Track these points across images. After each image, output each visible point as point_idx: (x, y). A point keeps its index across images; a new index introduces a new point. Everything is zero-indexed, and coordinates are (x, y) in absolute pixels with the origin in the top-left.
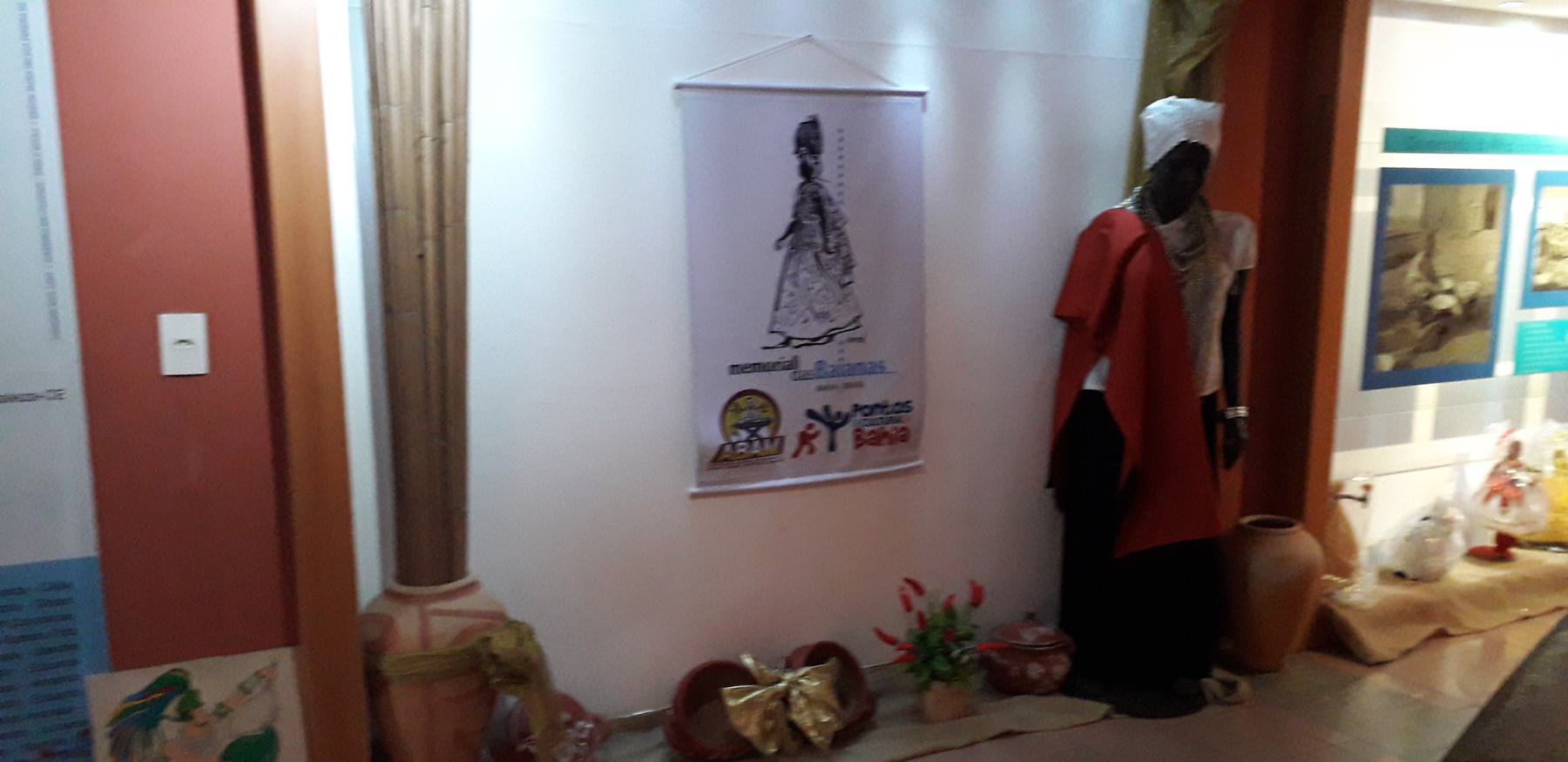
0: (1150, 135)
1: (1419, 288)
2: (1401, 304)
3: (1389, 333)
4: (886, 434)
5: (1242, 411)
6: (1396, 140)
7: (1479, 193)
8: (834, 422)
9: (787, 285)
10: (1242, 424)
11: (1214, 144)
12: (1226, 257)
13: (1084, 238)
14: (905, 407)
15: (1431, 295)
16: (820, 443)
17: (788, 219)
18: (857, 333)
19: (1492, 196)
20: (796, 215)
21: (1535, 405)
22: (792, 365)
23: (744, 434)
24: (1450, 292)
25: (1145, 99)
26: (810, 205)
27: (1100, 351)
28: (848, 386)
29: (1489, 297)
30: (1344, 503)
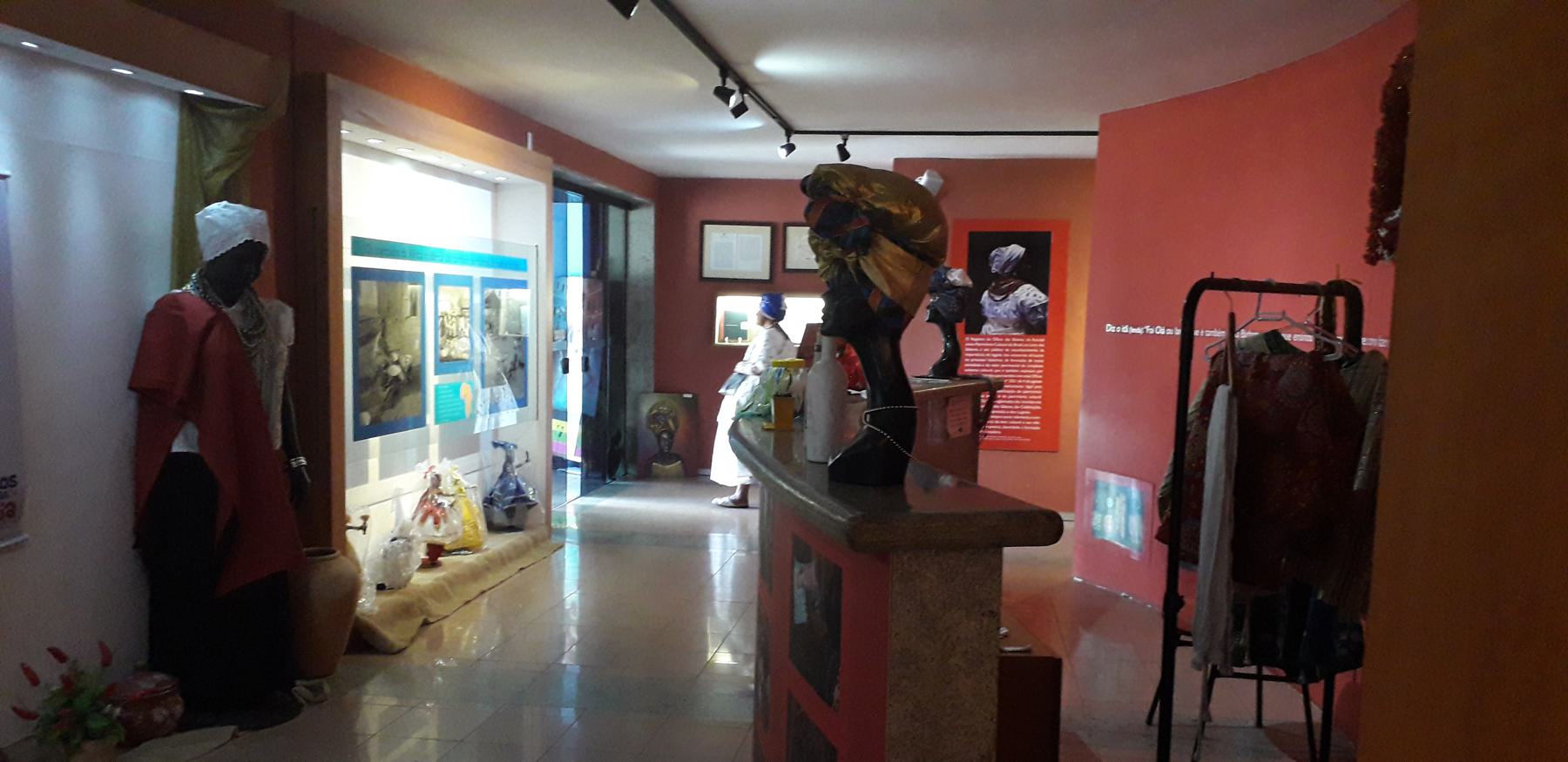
1: (380, 360)
2: (371, 372)
3: (366, 395)
5: (303, 461)
11: (267, 240)
15: (387, 366)
21: (434, 448)
24: (397, 363)
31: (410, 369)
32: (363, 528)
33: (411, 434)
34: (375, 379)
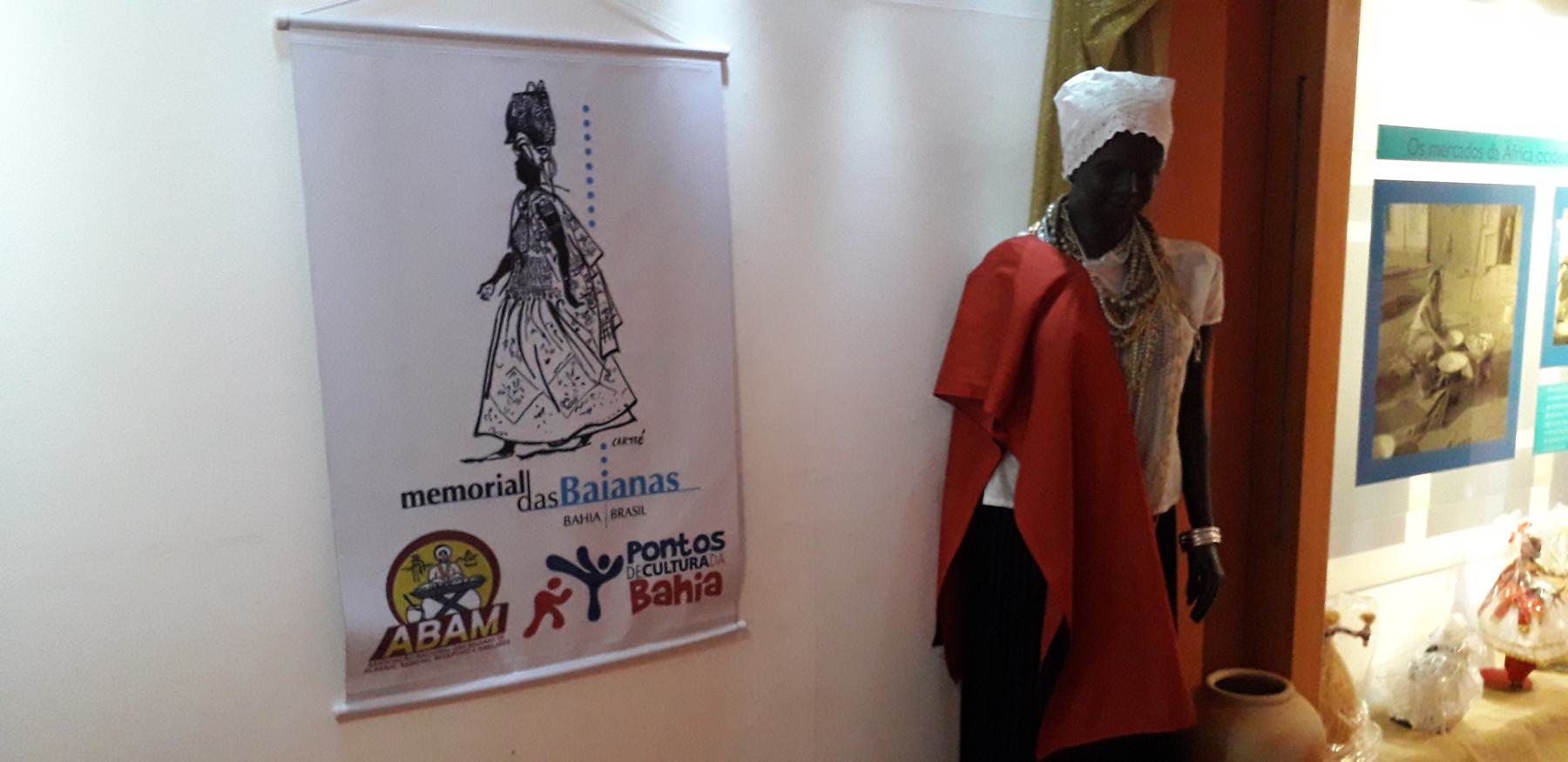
0: (1067, 124)
1: (1426, 343)
2: (1403, 366)
3: (1391, 405)
4: (687, 586)
5: (1215, 535)
6: (1393, 143)
7: (1492, 217)
8: (595, 573)
9: (503, 356)
10: (1214, 552)
12: (1184, 306)
13: (974, 279)
14: (716, 541)
15: (1438, 353)
16: (575, 609)
17: (503, 250)
18: (632, 431)
19: (1507, 221)
20: (512, 242)
21: (1540, 493)
22: (519, 486)
23: (432, 607)
24: (1462, 348)
25: (1056, 76)
26: (539, 226)
27: (1005, 450)
28: (617, 514)
29: (1508, 354)
30: (1339, 641)
31: (1488, 358)
32: (1365, 636)
33: (1493, 471)
34: (1412, 375)
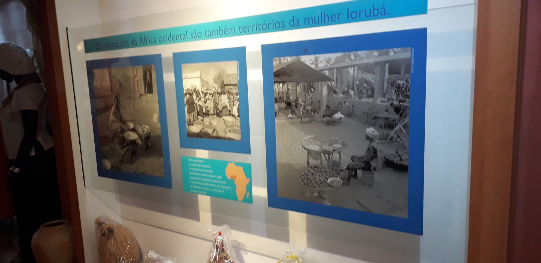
1: (117, 126)
6: (91, 45)
15: (123, 131)
19: (147, 74)
24: (134, 130)
